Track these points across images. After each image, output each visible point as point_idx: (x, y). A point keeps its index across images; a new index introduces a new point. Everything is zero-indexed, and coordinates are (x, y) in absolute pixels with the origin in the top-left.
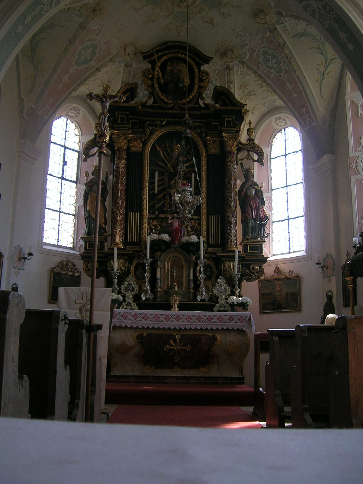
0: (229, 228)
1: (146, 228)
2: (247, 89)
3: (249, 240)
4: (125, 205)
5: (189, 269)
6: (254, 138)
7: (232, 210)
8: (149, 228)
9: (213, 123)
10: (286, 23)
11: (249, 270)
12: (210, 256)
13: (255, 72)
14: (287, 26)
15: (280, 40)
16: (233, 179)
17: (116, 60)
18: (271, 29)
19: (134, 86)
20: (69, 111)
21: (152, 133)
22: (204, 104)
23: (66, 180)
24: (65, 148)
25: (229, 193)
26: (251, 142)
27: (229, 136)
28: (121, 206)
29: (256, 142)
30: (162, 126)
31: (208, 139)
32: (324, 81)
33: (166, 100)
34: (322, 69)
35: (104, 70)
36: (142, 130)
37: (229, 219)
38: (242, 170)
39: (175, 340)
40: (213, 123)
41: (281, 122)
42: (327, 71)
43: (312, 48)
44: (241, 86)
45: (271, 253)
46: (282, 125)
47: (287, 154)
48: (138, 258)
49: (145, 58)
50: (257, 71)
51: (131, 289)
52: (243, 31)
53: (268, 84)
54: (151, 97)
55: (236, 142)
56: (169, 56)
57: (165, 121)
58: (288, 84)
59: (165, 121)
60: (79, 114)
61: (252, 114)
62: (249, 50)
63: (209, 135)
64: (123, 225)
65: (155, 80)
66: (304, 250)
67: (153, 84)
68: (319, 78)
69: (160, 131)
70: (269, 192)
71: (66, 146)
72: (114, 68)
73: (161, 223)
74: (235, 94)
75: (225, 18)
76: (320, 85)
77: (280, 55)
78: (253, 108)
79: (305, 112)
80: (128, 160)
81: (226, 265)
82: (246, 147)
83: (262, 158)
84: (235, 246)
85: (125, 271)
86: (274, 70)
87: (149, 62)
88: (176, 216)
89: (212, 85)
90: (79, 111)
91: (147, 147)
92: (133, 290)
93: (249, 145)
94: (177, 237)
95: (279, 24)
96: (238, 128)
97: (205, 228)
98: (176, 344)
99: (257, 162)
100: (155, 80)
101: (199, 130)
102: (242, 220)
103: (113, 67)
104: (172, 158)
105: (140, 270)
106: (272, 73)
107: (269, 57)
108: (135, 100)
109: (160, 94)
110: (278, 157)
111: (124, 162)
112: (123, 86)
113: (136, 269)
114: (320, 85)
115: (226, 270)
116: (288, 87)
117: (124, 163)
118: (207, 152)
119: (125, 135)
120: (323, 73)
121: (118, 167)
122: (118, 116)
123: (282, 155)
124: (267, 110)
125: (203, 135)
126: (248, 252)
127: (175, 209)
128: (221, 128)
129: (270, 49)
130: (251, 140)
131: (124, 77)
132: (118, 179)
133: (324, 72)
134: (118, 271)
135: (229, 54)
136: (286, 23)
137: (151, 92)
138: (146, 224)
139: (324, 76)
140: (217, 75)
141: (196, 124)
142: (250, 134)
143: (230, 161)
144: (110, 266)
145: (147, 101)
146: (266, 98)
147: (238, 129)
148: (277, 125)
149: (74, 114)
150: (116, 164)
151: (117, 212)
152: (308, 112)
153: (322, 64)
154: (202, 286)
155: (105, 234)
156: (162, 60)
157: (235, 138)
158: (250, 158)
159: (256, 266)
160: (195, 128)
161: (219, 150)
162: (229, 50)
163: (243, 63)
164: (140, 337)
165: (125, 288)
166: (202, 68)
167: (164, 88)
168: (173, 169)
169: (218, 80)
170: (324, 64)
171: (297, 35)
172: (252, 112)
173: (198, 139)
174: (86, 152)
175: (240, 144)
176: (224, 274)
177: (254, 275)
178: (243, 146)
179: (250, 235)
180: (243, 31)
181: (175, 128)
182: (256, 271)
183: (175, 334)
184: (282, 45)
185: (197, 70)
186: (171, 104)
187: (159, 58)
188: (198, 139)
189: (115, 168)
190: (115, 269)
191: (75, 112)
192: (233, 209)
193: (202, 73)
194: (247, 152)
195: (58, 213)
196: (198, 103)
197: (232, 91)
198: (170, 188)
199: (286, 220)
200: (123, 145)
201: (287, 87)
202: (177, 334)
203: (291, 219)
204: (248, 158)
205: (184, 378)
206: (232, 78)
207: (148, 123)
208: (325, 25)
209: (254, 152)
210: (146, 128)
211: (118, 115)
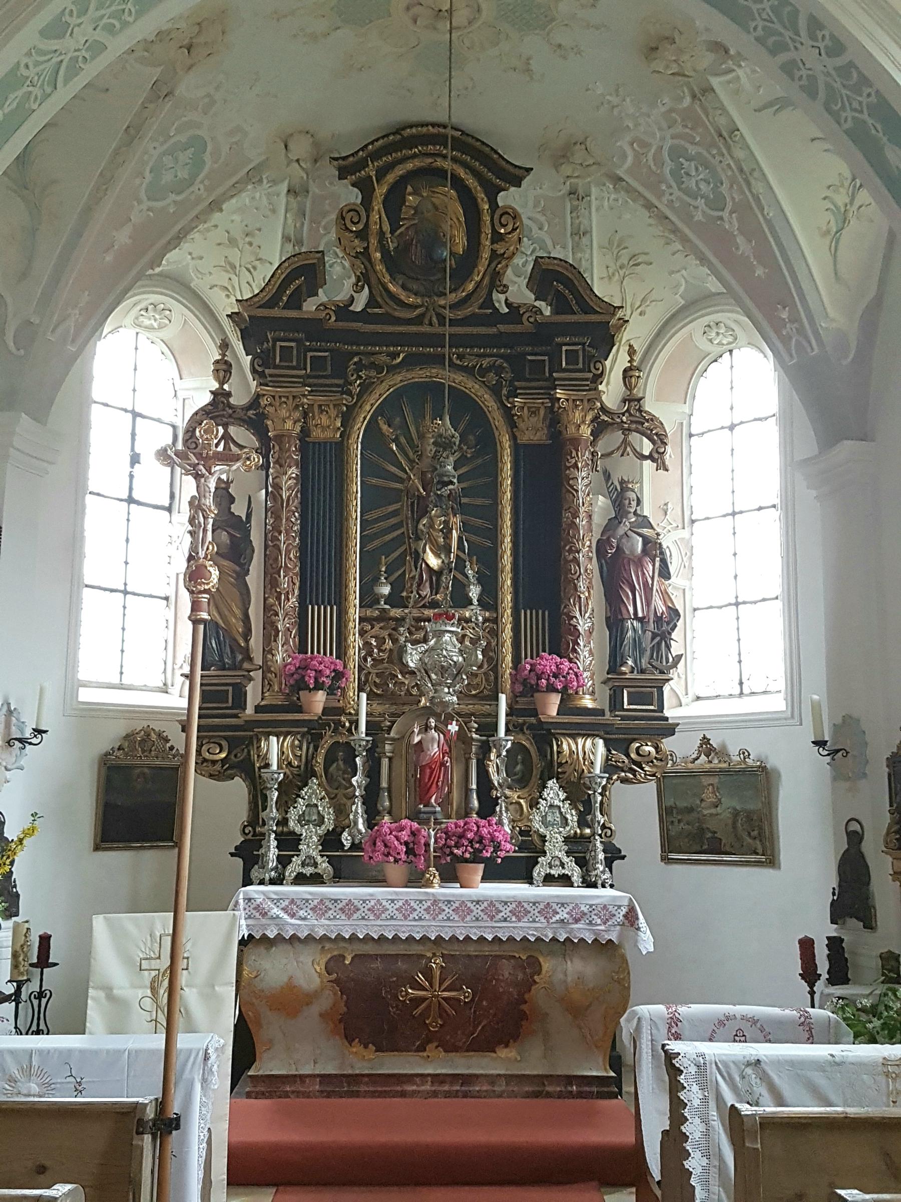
0: (573, 647)
1: (354, 647)
2: (626, 248)
3: (627, 676)
4: (300, 588)
5: (468, 760)
6: (641, 395)
7: (580, 598)
8: (363, 645)
9: (529, 358)
10: (740, 72)
11: (628, 755)
12: (524, 723)
13: (649, 206)
14: (744, 80)
15: (722, 121)
16: (582, 515)
17: (264, 177)
18: (695, 88)
19: (315, 261)
20: (142, 312)
21: (366, 388)
22: (508, 304)
23: (139, 503)
24: (135, 415)
25: (570, 551)
26: (633, 404)
27: (573, 398)
28: (288, 593)
29: (649, 406)
30: (392, 369)
31: (516, 404)
32: (844, 232)
33: (403, 295)
34: (841, 199)
35: (229, 205)
36: (341, 382)
37: (572, 622)
38: (608, 488)
39: (428, 973)
40: (529, 358)
41: (721, 336)
42: (857, 203)
43: (813, 140)
44: (610, 242)
45: (689, 692)
46: (725, 342)
47: (736, 425)
48: (335, 731)
49: (343, 174)
50: (657, 203)
51: (315, 817)
52: (617, 90)
53: (685, 240)
54: (363, 287)
55: (591, 412)
56: (410, 166)
57: (402, 356)
58: (740, 240)
59: (402, 356)
60: (170, 321)
61: (640, 314)
62: (632, 145)
63: (518, 391)
64: (294, 642)
65: (374, 241)
66: (780, 691)
67: (366, 249)
68: (833, 223)
69: (390, 383)
70: (684, 528)
71: (137, 410)
72: (260, 197)
73: (394, 632)
74: (592, 280)
75: (565, 58)
76: (833, 244)
77: (721, 162)
78: (643, 300)
79: (788, 318)
80: (303, 466)
81: (565, 746)
82: (618, 420)
83: (662, 450)
84: (588, 697)
85: (299, 767)
86: (703, 201)
87: (354, 185)
88: (433, 725)
89: (530, 242)
90: (168, 312)
91: (356, 428)
92: (321, 821)
93: (627, 414)
94: (434, 785)
95: (717, 75)
96: (598, 369)
97: (509, 643)
98: (431, 985)
99: (649, 461)
100: (374, 241)
101: (492, 377)
102: (608, 619)
103: (257, 195)
104: (420, 457)
105: (341, 763)
106: (696, 208)
107: (690, 165)
108: (322, 296)
109: (387, 278)
110: (709, 431)
111: (293, 471)
112: (284, 262)
113: (329, 760)
114: (833, 244)
115: (564, 761)
116: (741, 249)
117: (294, 475)
118: (514, 438)
119: (294, 397)
120: (843, 210)
121: (277, 487)
122: (274, 346)
123: (722, 428)
124: (683, 302)
125: (504, 392)
126: (625, 707)
127: (431, 594)
128: (551, 375)
129: (692, 143)
130: (632, 400)
131: (290, 221)
132: (278, 518)
133: (848, 207)
134: (282, 768)
135: (579, 155)
136: (740, 72)
137: (361, 273)
138: (354, 635)
139: (845, 219)
140: (543, 212)
141: (485, 362)
142: (631, 386)
143: (576, 466)
144: (259, 756)
145: (352, 300)
146: (679, 271)
147: (600, 372)
148: (711, 341)
149: (155, 320)
150: (273, 479)
151: (277, 608)
152: (795, 319)
153: (842, 186)
154: (501, 808)
155: (246, 665)
156: (391, 178)
157: (589, 400)
158: (628, 449)
159: (647, 745)
160: (483, 372)
161: (546, 432)
162: (575, 144)
163: (617, 180)
164: (334, 964)
165: (299, 816)
166: (502, 199)
167: (392, 263)
168: (423, 488)
169: (546, 228)
170: (846, 184)
171: (770, 104)
172: (639, 310)
173: (489, 402)
174: (190, 441)
175: (604, 413)
176: (558, 773)
177: (642, 769)
178: (612, 419)
179: (630, 662)
180: (617, 90)
181: (428, 374)
182: (646, 759)
183: (429, 955)
184: (725, 134)
185: (487, 207)
186: (417, 307)
187: (381, 174)
188: (489, 402)
189: (270, 489)
190: (274, 767)
191: (157, 317)
192: (582, 596)
193: (501, 216)
194: (623, 433)
195: (122, 595)
196: (488, 302)
197: (583, 267)
198: (418, 538)
199: (730, 604)
200: (289, 425)
201: (737, 248)
202: (434, 955)
203: (744, 603)
204: (625, 448)
205: (454, 1078)
206: (585, 222)
207: (356, 359)
208: (846, 121)
209: (643, 434)
210: (352, 375)
211: (275, 340)
